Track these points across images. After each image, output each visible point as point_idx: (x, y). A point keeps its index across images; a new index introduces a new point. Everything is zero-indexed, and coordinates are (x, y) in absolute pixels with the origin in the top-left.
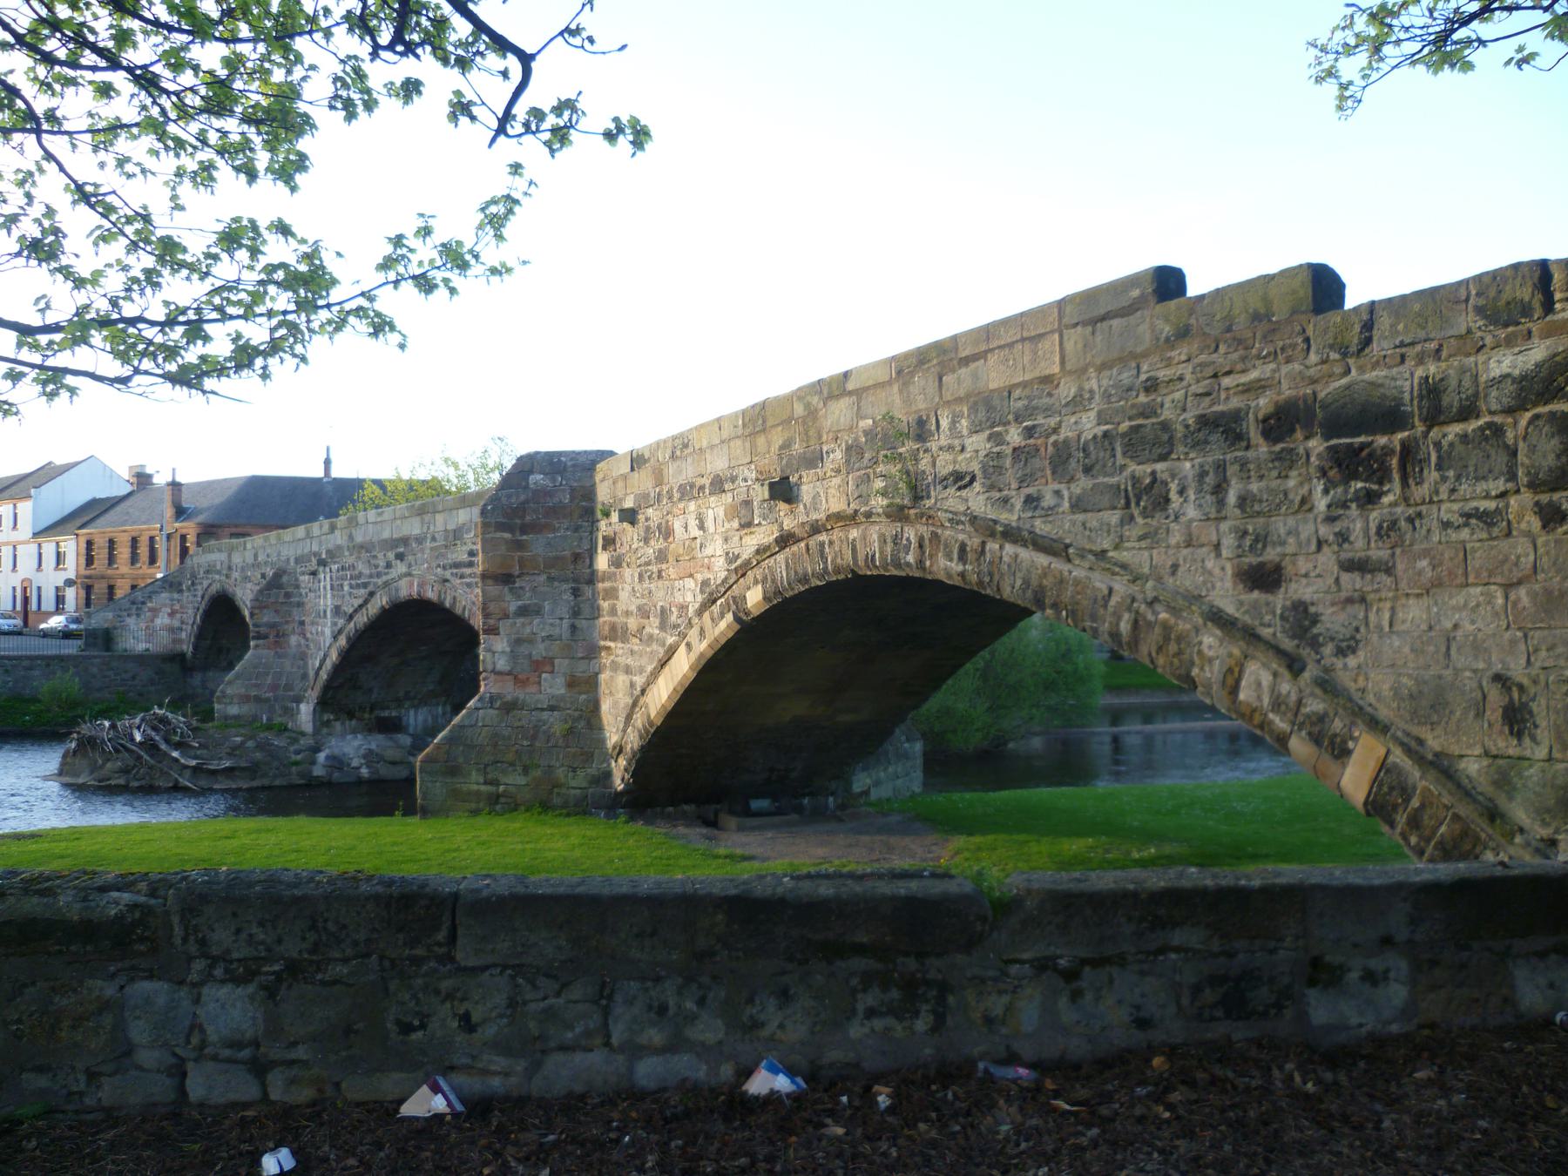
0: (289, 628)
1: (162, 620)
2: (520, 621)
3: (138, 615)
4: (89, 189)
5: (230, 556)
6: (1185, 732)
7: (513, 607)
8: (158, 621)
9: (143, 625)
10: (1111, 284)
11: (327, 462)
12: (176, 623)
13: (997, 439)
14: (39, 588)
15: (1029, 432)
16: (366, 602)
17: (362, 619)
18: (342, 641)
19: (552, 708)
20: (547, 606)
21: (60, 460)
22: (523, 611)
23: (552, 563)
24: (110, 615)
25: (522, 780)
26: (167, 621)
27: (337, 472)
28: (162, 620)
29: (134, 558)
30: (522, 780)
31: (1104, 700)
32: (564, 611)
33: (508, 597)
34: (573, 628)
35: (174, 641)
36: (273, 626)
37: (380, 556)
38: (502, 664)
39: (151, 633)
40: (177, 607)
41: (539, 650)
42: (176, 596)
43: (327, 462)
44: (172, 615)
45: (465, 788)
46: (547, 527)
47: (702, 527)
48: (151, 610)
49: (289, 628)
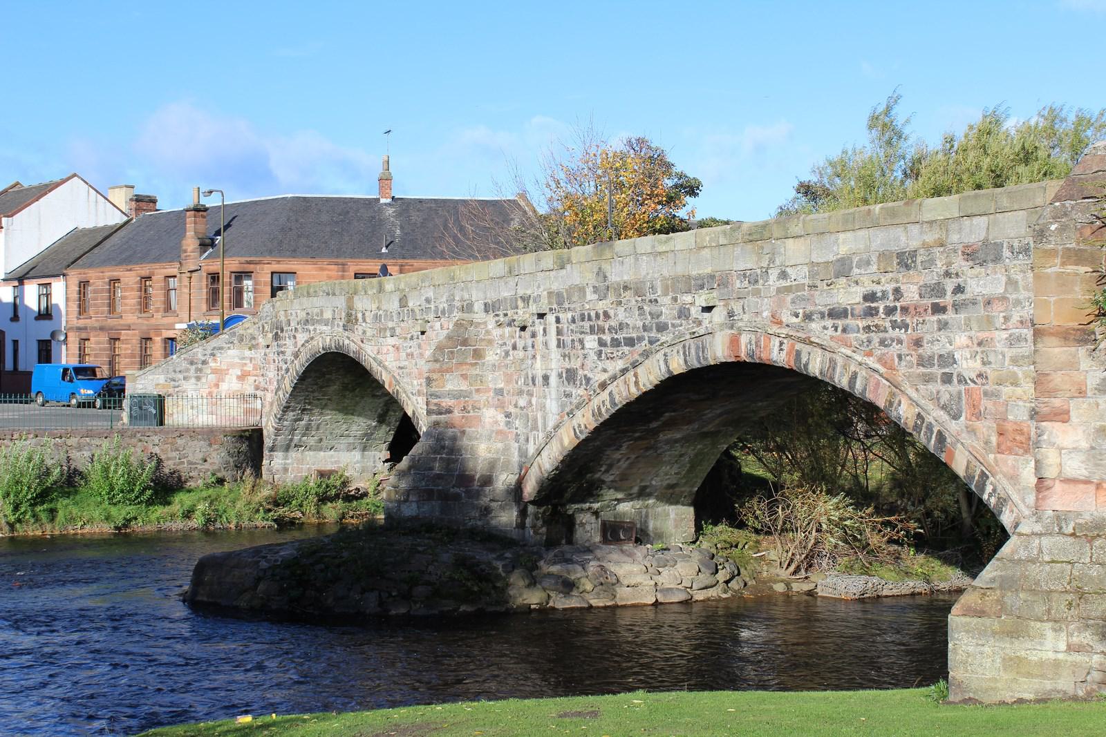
0: (481, 398)
1: (231, 384)
3: (198, 379)
5: (350, 300)
6: (67, 355)
8: (224, 387)
9: (205, 392)
12: (250, 390)
14: (15, 342)
28: (231, 384)
29: (144, 304)
31: (218, 364)
35: (247, 412)
36: (458, 395)
37: (667, 300)
38: (1075, 466)
39: (214, 399)
40: (249, 368)
42: (247, 353)
44: (242, 378)
45: (1034, 657)
48: (215, 371)
49: (481, 398)
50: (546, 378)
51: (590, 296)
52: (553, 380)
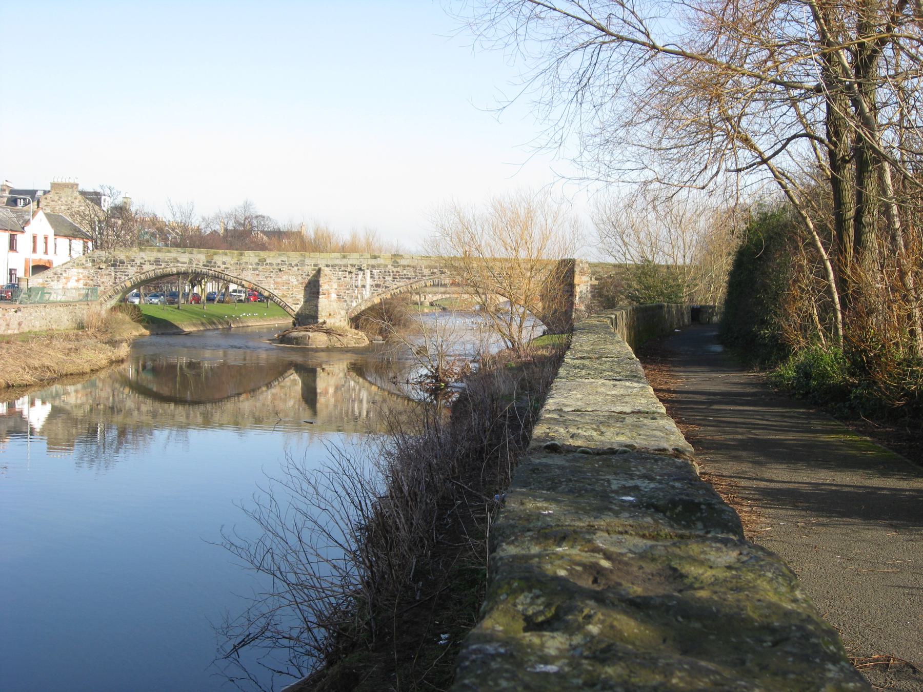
50: (364, 286)
51: (390, 266)
52: (368, 287)
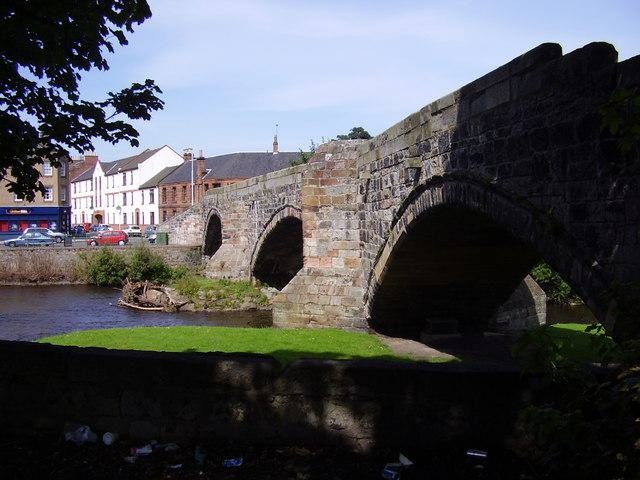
2: (321, 230)
4: (101, 277)
7: (318, 223)
10: (500, 69)
11: (276, 144)
13: (489, 136)
15: (500, 133)
16: (271, 219)
17: (269, 228)
18: (262, 239)
19: (337, 276)
20: (334, 223)
21: (152, 149)
22: (323, 225)
23: (336, 200)
24: (167, 227)
25: (322, 312)
26: (193, 229)
27: (281, 149)
30: (322, 312)
32: (343, 225)
33: (316, 218)
34: (347, 233)
38: (314, 253)
41: (332, 245)
43: (276, 144)
46: (335, 182)
47: (392, 182)
